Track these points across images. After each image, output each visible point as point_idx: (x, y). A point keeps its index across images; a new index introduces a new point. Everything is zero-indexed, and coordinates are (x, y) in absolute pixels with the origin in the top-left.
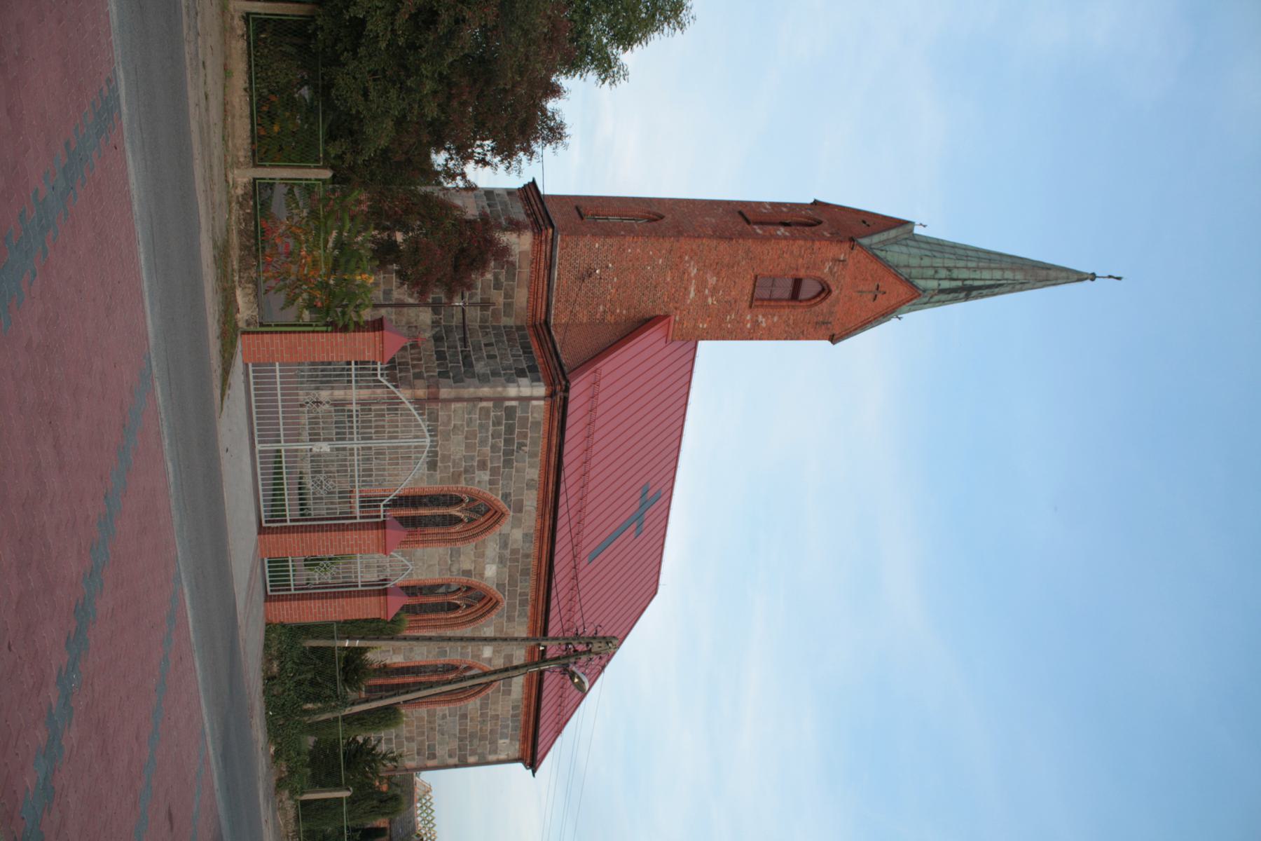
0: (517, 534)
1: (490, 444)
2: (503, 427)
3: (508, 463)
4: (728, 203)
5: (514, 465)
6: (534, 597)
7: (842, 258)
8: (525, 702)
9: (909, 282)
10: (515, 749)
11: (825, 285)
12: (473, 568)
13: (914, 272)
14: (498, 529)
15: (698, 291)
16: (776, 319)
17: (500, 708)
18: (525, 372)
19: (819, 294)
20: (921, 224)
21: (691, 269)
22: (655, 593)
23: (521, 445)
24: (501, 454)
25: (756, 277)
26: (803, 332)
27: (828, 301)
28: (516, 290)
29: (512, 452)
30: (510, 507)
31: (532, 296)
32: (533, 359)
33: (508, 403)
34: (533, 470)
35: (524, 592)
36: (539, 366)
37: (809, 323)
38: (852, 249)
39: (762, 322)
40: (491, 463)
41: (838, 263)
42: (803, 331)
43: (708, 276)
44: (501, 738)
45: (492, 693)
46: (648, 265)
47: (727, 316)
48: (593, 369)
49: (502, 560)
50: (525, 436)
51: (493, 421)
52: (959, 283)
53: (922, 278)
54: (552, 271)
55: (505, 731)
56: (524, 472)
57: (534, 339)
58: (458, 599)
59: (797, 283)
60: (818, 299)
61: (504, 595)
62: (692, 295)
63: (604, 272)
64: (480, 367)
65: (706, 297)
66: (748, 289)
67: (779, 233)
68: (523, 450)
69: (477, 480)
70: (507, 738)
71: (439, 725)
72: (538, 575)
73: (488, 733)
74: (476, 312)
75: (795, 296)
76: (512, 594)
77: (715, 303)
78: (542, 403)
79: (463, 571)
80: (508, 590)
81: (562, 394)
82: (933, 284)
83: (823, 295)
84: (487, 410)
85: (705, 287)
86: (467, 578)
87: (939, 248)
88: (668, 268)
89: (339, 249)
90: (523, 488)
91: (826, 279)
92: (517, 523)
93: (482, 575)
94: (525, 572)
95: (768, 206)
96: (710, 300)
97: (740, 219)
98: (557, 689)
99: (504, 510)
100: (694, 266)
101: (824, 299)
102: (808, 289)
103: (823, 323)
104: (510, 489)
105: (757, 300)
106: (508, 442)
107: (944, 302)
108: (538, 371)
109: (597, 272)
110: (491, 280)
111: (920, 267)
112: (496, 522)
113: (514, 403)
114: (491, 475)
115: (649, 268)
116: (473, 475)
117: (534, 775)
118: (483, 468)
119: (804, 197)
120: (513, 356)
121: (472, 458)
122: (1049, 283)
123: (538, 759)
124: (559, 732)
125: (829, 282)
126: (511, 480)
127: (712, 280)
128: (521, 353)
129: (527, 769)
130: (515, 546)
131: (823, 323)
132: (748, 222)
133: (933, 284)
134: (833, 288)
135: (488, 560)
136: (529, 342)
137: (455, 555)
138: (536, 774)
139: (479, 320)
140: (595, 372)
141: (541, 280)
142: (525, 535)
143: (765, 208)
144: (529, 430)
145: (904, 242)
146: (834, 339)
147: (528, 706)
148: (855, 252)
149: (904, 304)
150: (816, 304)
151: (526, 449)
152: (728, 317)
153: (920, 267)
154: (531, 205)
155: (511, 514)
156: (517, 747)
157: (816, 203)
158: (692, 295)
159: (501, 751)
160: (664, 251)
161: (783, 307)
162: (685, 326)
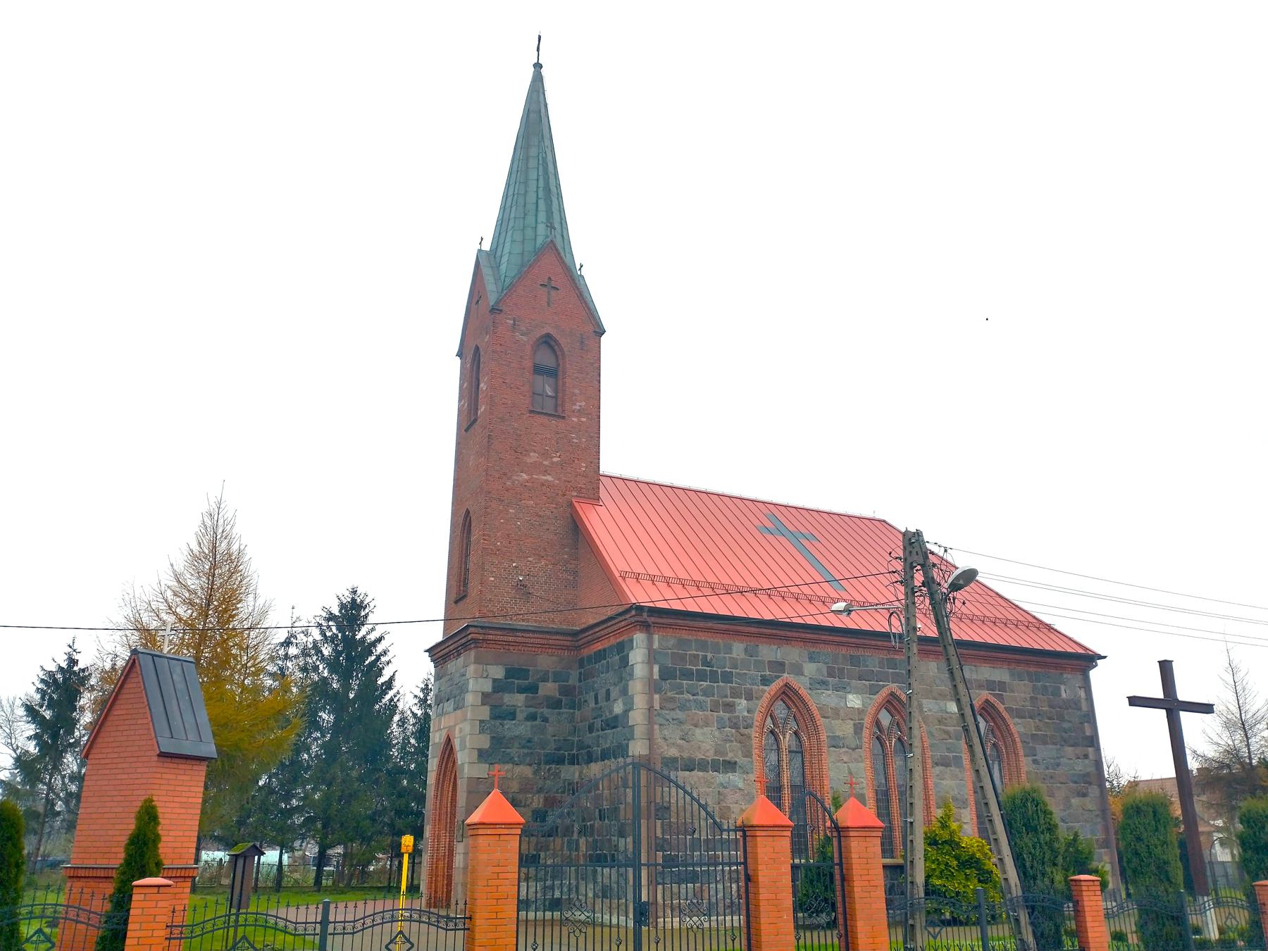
0: (810, 668)
1: (703, 698)
2: (685, 682)
3: (727, 678)
4: (458, 444)
5: (729, 670)
6: (885, 652)
7: (512, 322)
8: (1013, 666)
9: (539, 253)
10: (1073, 679)
11: (541, 341)
12: (852, 722)
13: (529, 247)
14: (803, 692)
15: (546, 472)
16: (577, 391)
17: (1023, 695)
18: (623, 656)
19: (552, 348)
20: (480, 243)
21: (521, 478)
22: (884, 521)
23: (706, 663)
24: (716, 684)
25: (531, 412)
26: (592, 364)
27: (558, 337)
28: (539, 668)
29: (714, 673)
30: (778, 677)
31: (547, 650)
32: (611, 648)
33: (656, 676)
34: (734, 649)
35: (879, 663)
36: (618, 641)
37: (582, 357)
38: (501, 311)
39: (580, 406)
40: (726, 696)
41: (516, 327)
42: (590, 363)
43: (529, 460)
44: (1060, 696)
45: (1004, 704)
46: (515, 525)
47: (573, 442)
48: (620, 580)
49: (842, 688)
50: (696, 656)
51: (677, 693)
52: (541, 203)
53: (535, 239)
54: (519, 627)
55: (1050, 690)
56: (737, 659)
57: (592, 647)
58: (890, 741)
59: (538, 370)
60: (556, 347)
61: (884, 686)
62: (549, 478)
63: (522, 571)
64: (618, 708)
65: (553, 463)
66: (544, 419)
67: (484, 388)
68: (711, 659)
69: (746, 714)
70: (1059, 689)
71: (1047, 768)
72: (857, 646)
73: (1054, 711)
74: (563, 713)
75: (553, 373)
76: (883, 677)
77: (558, 454)
78: (656, 637)
79: (856, 733)
80: (877, 681)
81: (645, 615)
82: (541, 229)
83: (552, 343)
84: (663, 700)
85: (542, 463)
86: (864, 729)
87: (505, 223)
88: (519, 503)
89: (366, 873)
90: (755, 660)
91: (535, 339)
92: (798, 671)
93: (860, 712)
94: (854, 661)
95: (462, 403)
96: (555, 460)
97: (472, 430)
98: (996, 629)
99: (782, 684)
100: (517, 476)
101: (556, 341)
102: (546, 359)
103: (582, 343)
104: (757, 676)
105: (556, 412)
106: (702, 676)
107: (561, 219)
108: (623, 641)
109: (521, 579)
110: (526, 697)
111: (523, 242)
112: (796, 693)
113: (656, 668)
114: (741, 698)
115: (519, 523)
116: (741, 718)
117: (1105, 657)
118: (732, 706)
119: (453, 367)
120: (608, 672)
121: (720, 720)
122: (543, 110)
123: (1083, 652)
124: (1049, 628)
125: (538, 336)
126: (745, 674)
127: (533, 457)
128: (605, 662)
129: (1096, 665)
130: (825, 672)
131: (582, 342)
132: (475, 420)
133: (541, 229)
134: (544, 331)
135: (842, 704)
136: (595, 653)
137: (836, 743)
138: (1103, 654)
139: (571, 711)
140: (624, 579)
141: (527, 640)
142: (812, 659)
143: (464, 405)
144: (688, 653)
145: (498, 260)
146: (600, 332)
147: (1018, 662)
148: (504, 308)
149: (564, 262)
150: (562, 350)
151: (709, 656)
152: (575, 441)
153: (523, 242)
154: (449, 652)
155: (785, 675)
156: (1069, 676)
157: (460, 354)
158: (549, 478)
159: (1075, 696)
160: (501, 507)
161: (564, 383)
162: (583, 486)
